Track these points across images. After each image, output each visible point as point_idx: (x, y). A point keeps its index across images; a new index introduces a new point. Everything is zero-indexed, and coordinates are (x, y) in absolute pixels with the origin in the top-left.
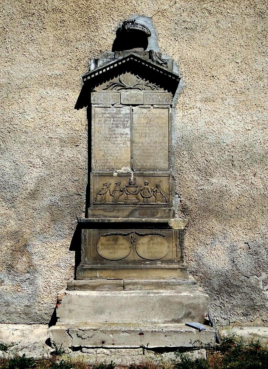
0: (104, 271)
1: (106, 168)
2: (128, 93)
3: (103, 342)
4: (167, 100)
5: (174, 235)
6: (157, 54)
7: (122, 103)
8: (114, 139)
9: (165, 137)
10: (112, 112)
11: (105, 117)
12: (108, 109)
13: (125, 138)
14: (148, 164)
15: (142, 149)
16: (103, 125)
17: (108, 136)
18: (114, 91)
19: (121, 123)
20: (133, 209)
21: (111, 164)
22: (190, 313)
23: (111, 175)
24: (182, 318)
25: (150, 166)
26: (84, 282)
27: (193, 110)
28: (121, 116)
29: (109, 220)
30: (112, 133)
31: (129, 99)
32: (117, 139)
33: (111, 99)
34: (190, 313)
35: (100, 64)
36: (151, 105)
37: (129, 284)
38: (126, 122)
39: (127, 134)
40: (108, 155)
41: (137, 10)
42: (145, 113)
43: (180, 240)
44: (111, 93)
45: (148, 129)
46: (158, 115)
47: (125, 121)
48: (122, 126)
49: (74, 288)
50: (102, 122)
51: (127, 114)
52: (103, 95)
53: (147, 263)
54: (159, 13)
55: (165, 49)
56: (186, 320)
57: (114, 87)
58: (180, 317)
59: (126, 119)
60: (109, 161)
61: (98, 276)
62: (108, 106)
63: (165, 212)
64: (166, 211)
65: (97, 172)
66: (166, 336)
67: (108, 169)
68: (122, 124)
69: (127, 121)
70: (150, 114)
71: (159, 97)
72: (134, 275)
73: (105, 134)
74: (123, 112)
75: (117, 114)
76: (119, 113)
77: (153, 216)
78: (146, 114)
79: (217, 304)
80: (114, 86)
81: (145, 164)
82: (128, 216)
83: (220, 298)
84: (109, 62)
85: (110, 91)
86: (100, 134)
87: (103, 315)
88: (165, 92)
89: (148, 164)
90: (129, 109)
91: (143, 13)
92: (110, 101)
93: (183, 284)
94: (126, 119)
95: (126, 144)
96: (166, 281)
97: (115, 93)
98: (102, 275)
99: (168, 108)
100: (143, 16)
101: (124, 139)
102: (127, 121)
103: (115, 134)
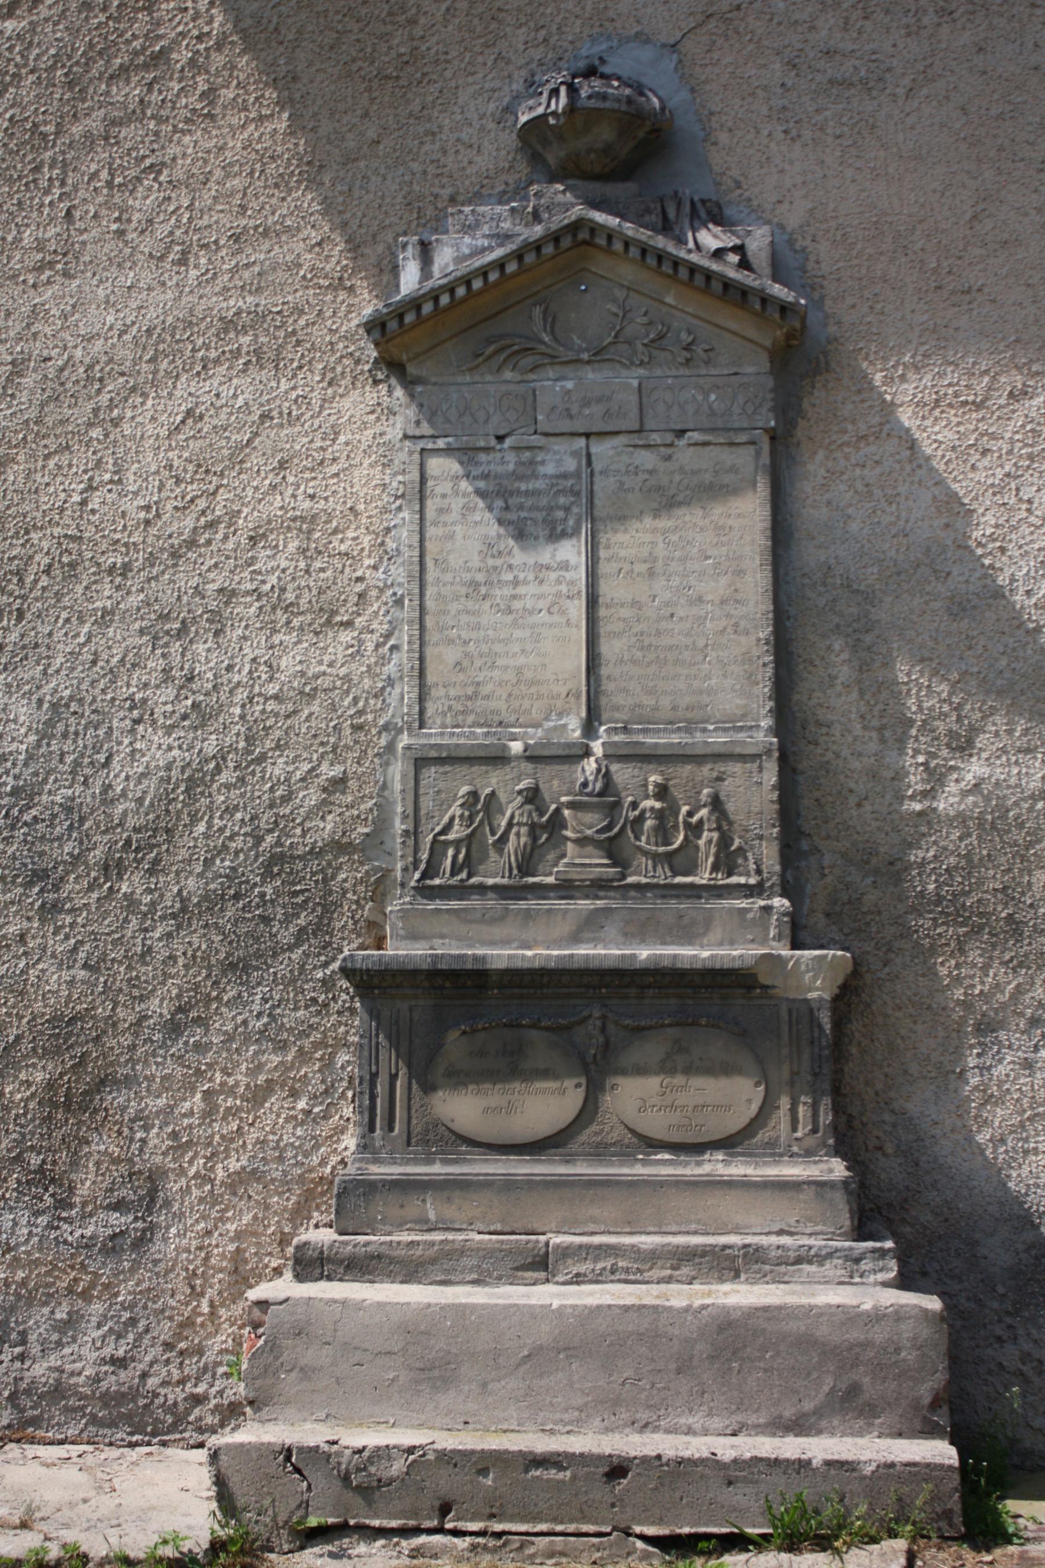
0: (457, 1193)
1: (471, 719)
2: (569, 385)
3: (445, 1510)
4: (750, 409)
5: (785, 1028)
6: (699, 205)
7: (540, 428)
8: (507, 591)
9: (740, 573)
10: (500, 469)
11: (464, 496)
12: (483, 457)
13: (558, 582)
14: (665, 702)
15: (635, 630)
16: (458, 528)
17: (480, 577)
18: (508, 375)
19: (540, 516)
20: (597, 909)
21: (493, 704)
22: (854, 1390)
23: (498, 759)
24: (818, 1412)
25: (674, 708)
26: (367, 1244)
27: (873, 448)
28: (540, 484)
29: (483, 958)
30: (498, 562)
31: (575, 409)
32: (521, 590)
33: (491, 411)
34: (854, 1390)
35: (446, 260)
36: (674, 431)
37: (566, 1252)
38: (560, 514)
39: (565, 566)
40: (478, 663)
41: (611, 14)
42: (650, 467)
43: (816, 1050)
44: (492, 389)
45: (661, 539)
46: (708, 477)
47: (559, 508)
48: (543, 532)
49: (319, 1271)
50: (454, 516)
51: (564, 476)
52: (455, 396)
53: (659, 1157)
54: (712, 24)
55: (741, 178)
56: (836, 1422)
57: (505, 360)
58: (808, 1406)
59: (562, 500)
60: (485, 690)
61: (432, 1215)
62: (482, 444)
63: (744, 920)
64: (750, 916)
65: (433, 742)
66: (730, 1483)
67: (481, 726)
68: (544, 521)
69: (567, 509)
70: (672, 473)
71: (713, 397)
72: (595, 1211)
73: (469, 570)
74: (550, 469)
75: (521, 478)
76: (528, 470)
77: (688, 934)
78: (651, 472)
79: (1005, 1364)
80: (509, 351)
81: (649, 701)
82: (575, 938)
83: (1021, 1332)
84: (483, 250)
85: (488, 378)
86: (444, 571)
87: (452, 1393)
88: (736, 374)
89: (665, 702)
90: (575, 454)
91: (639, 28)
92: (486, 421)
93: (830, 1255)
94: (562, 500)
95: (562, 612)
96: (749, 1240)
97: (511, 387)
98: (450, 1212)
99: (753, 443)
100: (642, 38)
101: (554, 590)
102: (567, 509)
103: (510, 566)
